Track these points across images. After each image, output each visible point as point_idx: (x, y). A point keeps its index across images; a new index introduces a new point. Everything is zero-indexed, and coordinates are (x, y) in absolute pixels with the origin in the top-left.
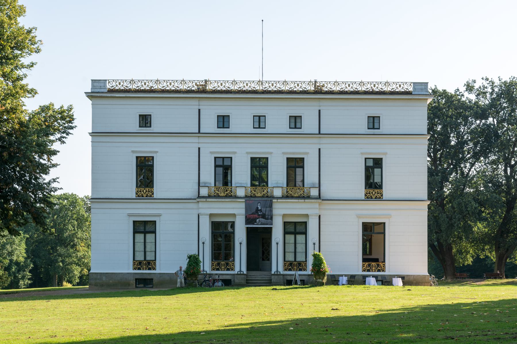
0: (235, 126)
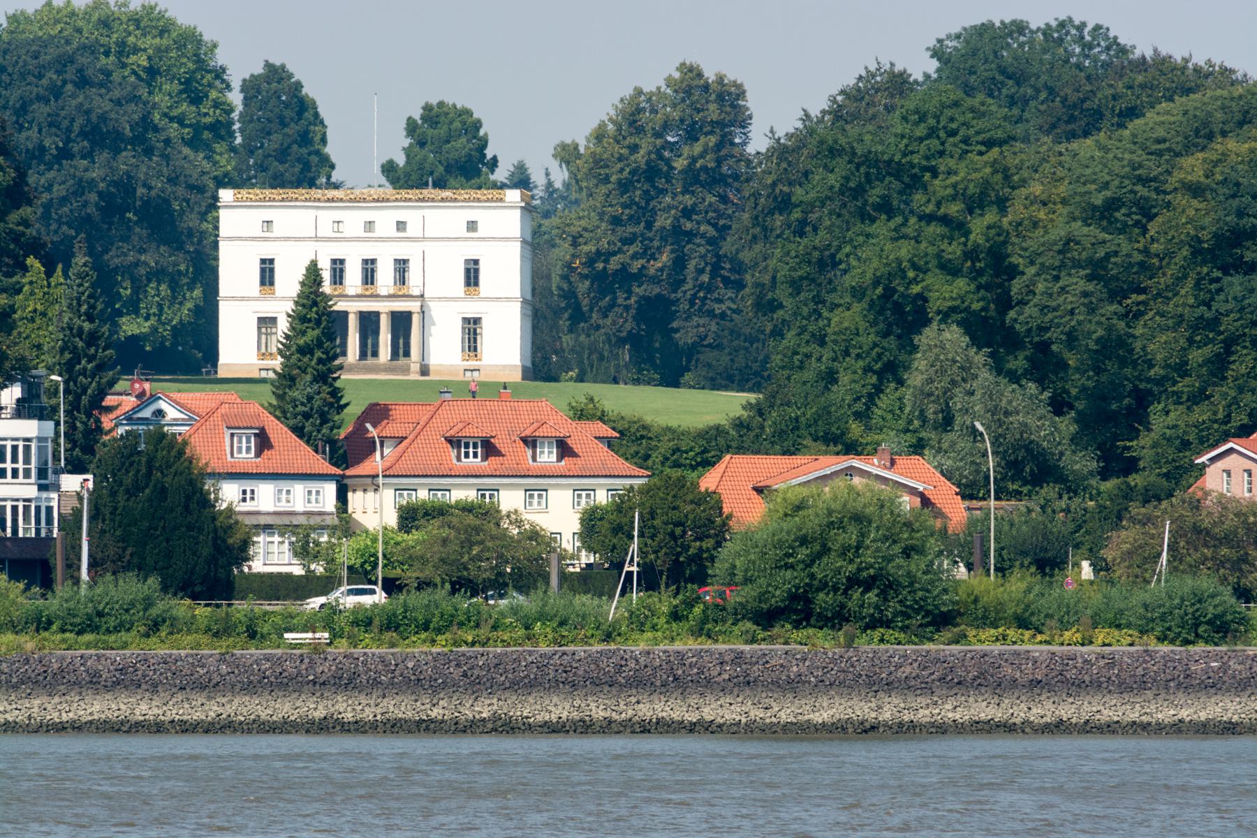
0: (379, 231)
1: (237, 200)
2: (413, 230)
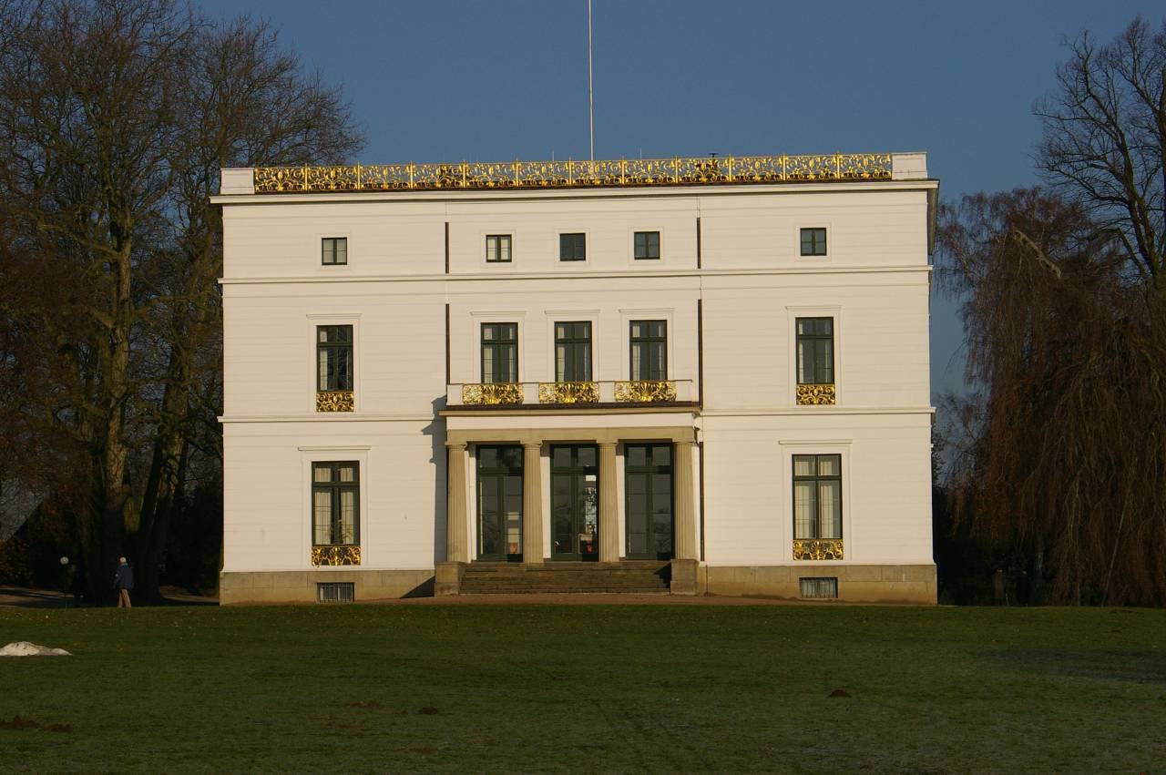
1: (263, 191)
2: (676, 251)
